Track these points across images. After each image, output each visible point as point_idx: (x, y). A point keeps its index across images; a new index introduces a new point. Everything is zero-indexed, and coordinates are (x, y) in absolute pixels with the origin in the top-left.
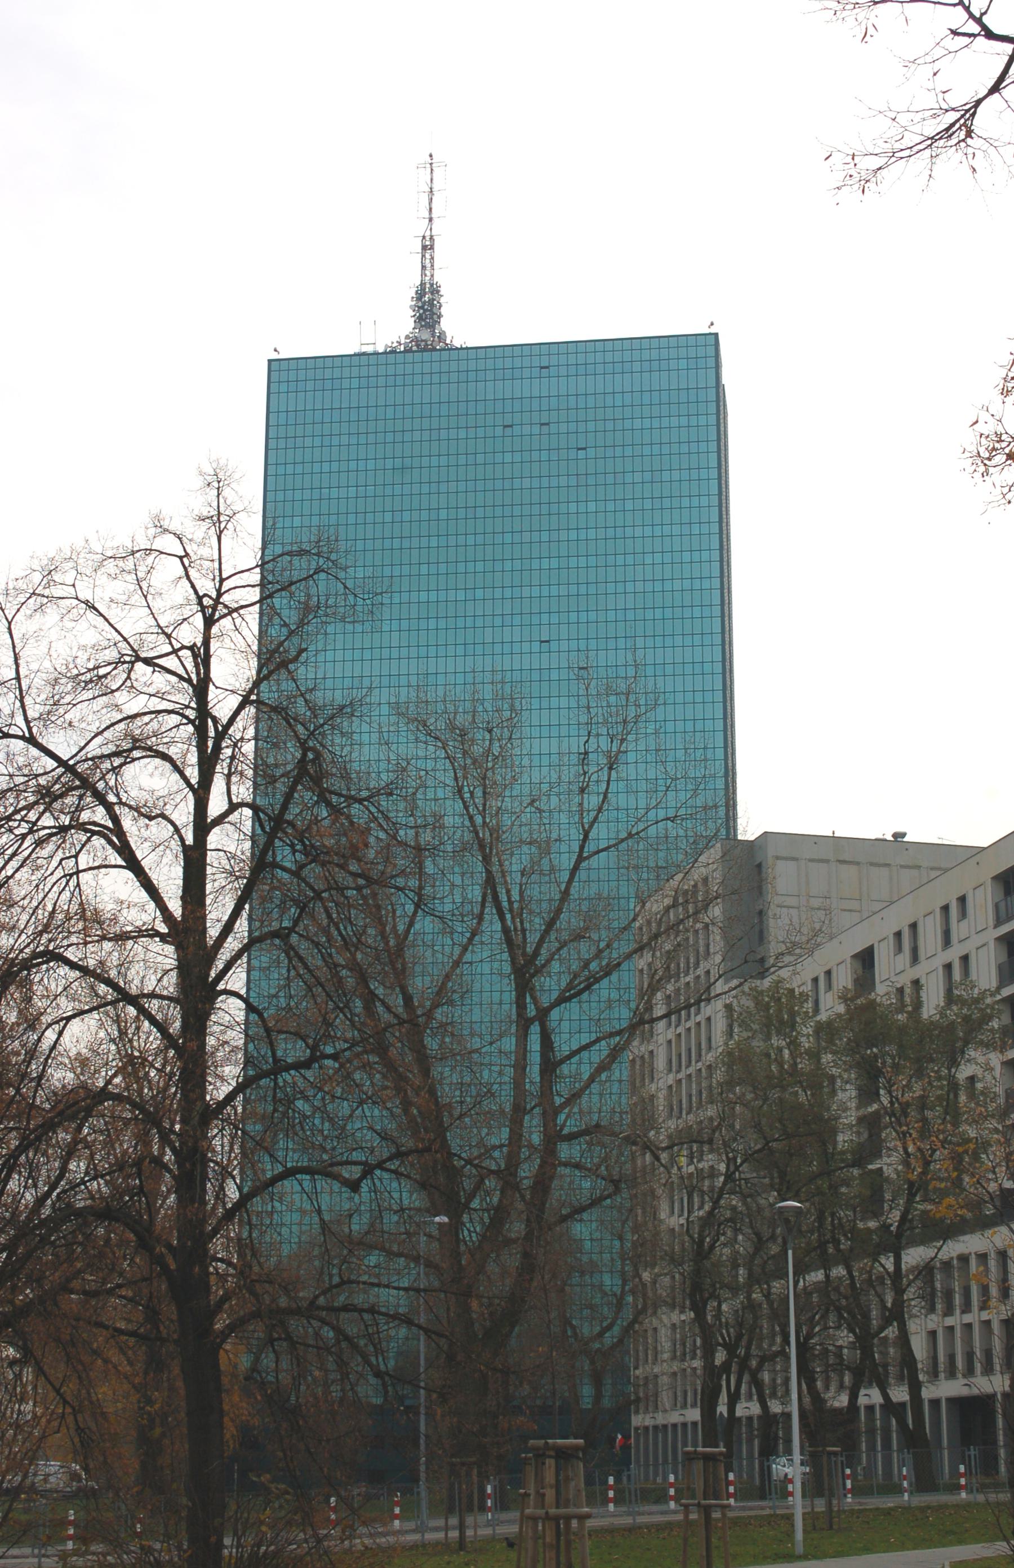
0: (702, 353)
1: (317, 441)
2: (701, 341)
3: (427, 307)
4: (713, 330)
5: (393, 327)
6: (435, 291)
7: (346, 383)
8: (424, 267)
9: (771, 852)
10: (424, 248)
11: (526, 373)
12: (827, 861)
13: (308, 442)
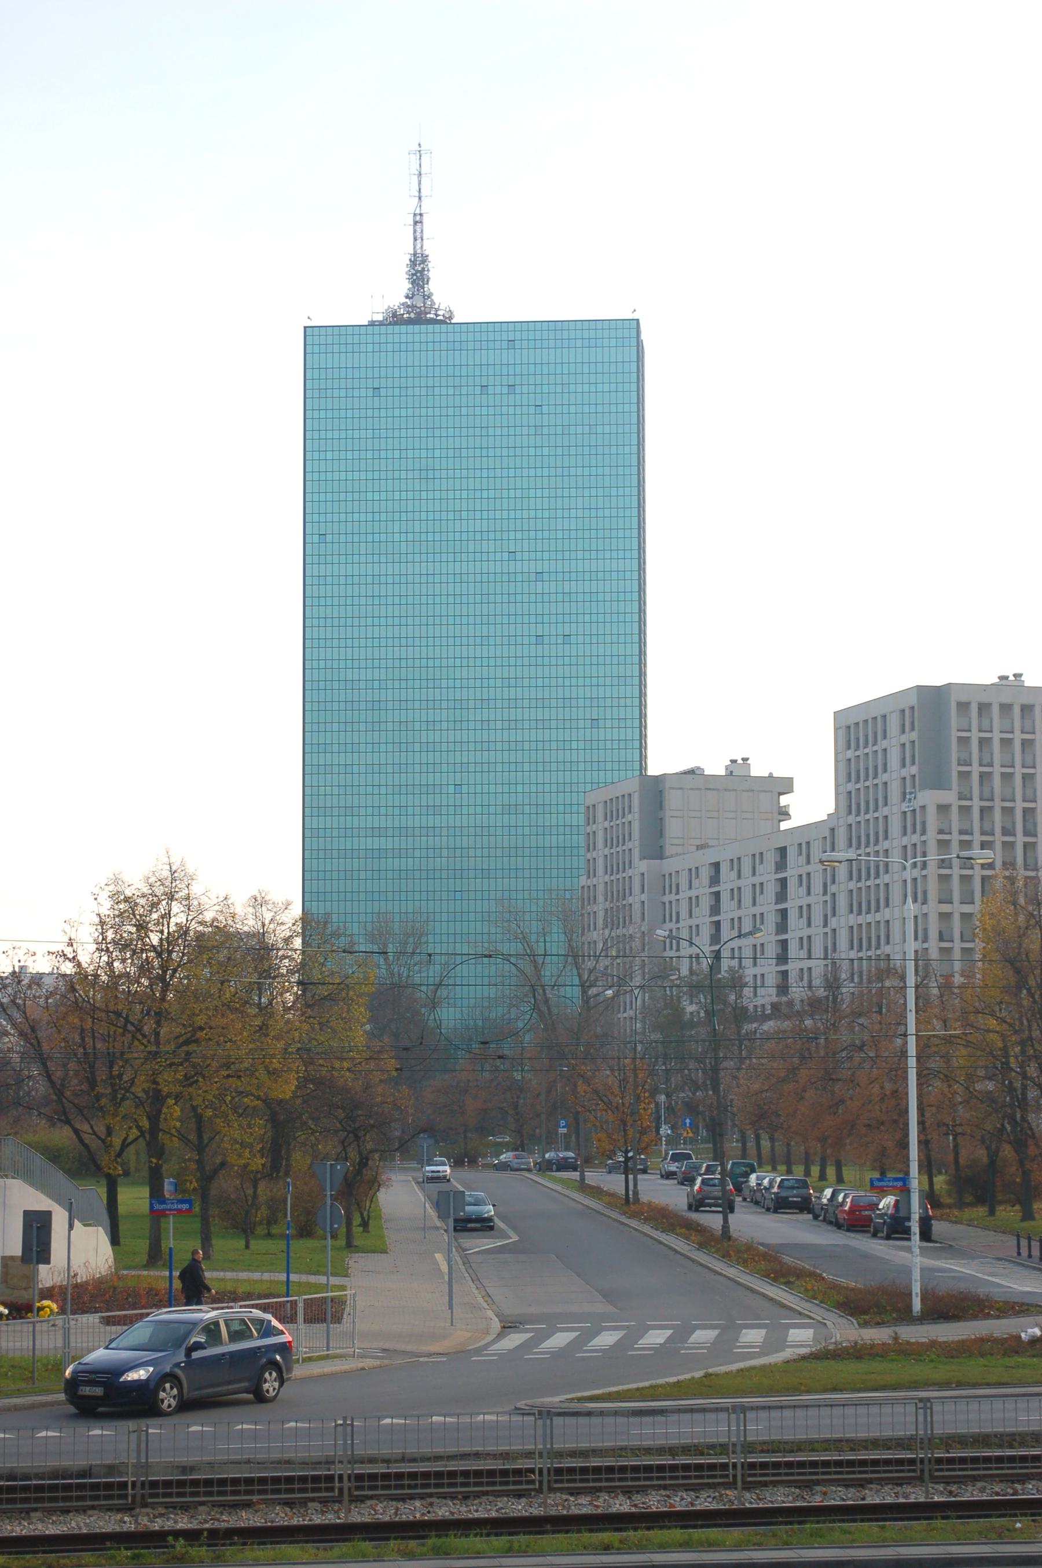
0: (628, 332)
1: (343, 393)
2: (627, 325)
3: (418, 273)
4: (635, 316)
5: (395, 293)
6: (424, 259)
7: (363, 348)
8: (415, 239)
9: (667, 785)
10: (416, 223)
11: (498, 345)
12: (699, 789)
13: (336, 393)
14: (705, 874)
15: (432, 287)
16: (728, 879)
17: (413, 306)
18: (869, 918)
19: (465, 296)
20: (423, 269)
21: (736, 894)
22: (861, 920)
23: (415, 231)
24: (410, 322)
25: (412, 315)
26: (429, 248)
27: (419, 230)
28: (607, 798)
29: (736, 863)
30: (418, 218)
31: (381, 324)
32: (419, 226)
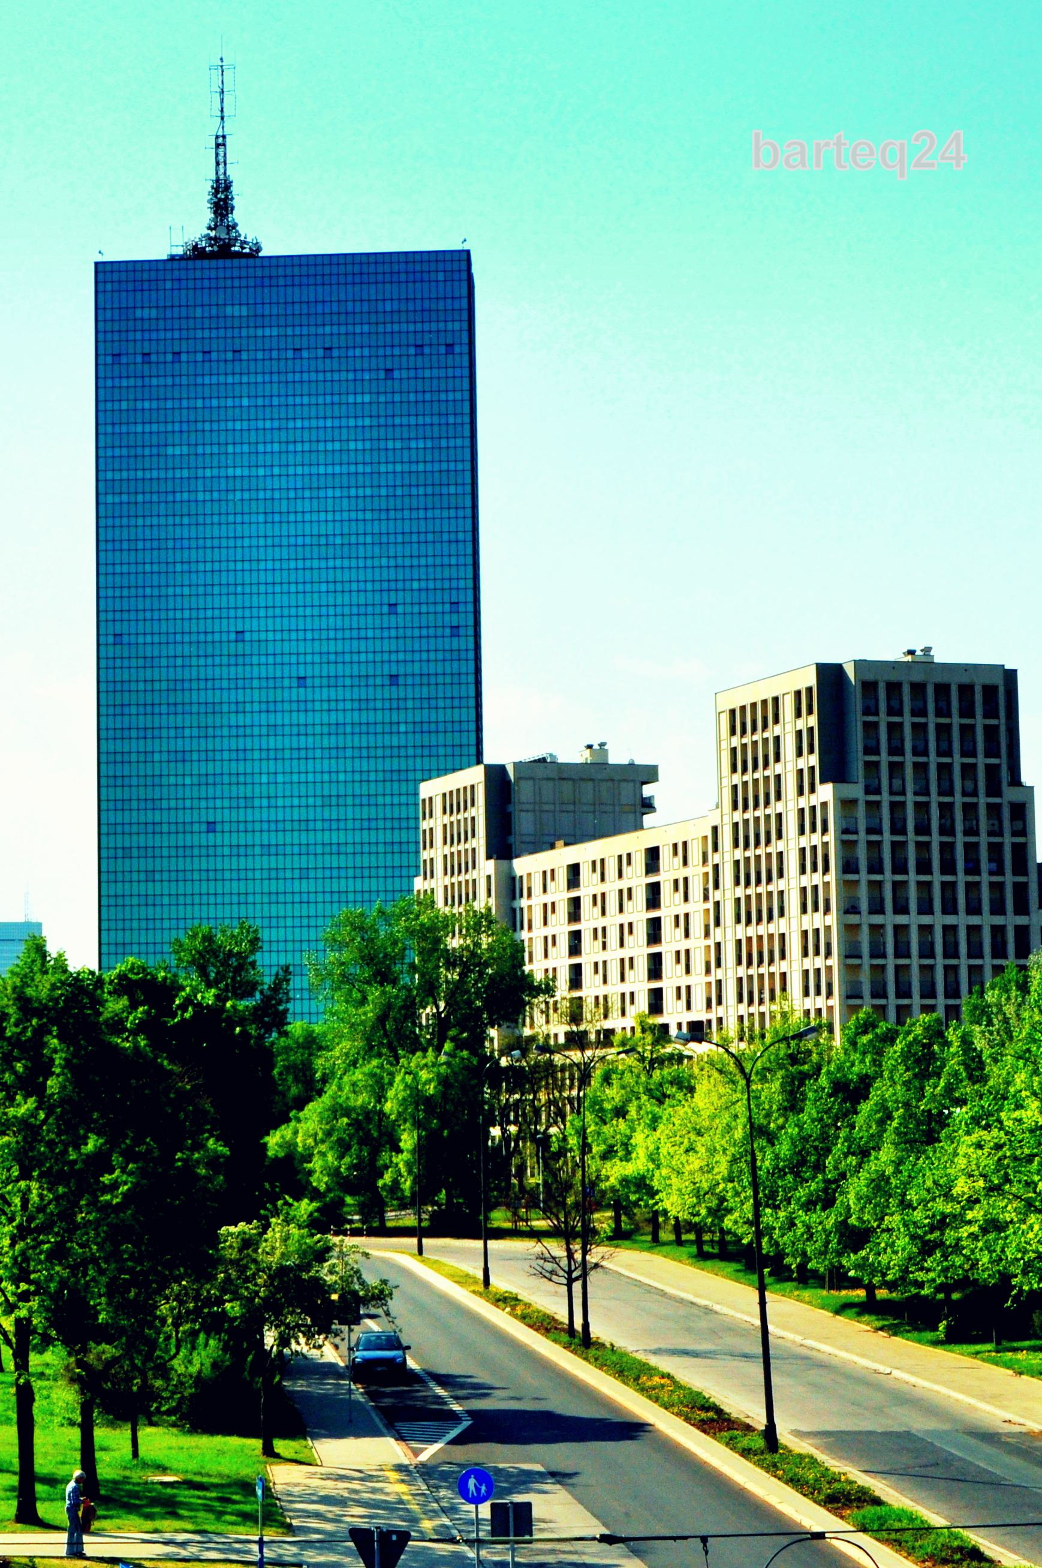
3: (222, 202)
5: (194, 225)
6: (228, 187)
8: (218, 164)
10: (218, 146)
12: (553, 779)
14: (562, 876)
15: (237, 216)
16: (670, 869)
17: (215, 239)
18: (762, 930)
19: (273, 228)
20: (227, 197)
21: (600, 901)
22: (751, 931)
23: (217, 155)
24: (212, 256)
25: (216, 248)
26: (233, 173)
27: (222, 154)
28: (447, 791)
29: (682, 850)
30: (220, 140)
31: (182, 258)
32: (221, 150)
